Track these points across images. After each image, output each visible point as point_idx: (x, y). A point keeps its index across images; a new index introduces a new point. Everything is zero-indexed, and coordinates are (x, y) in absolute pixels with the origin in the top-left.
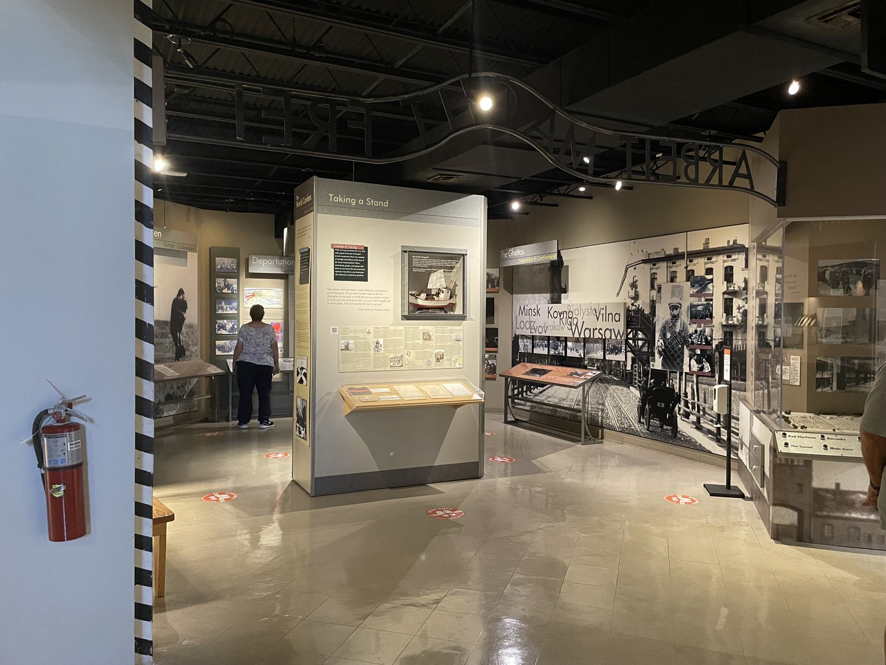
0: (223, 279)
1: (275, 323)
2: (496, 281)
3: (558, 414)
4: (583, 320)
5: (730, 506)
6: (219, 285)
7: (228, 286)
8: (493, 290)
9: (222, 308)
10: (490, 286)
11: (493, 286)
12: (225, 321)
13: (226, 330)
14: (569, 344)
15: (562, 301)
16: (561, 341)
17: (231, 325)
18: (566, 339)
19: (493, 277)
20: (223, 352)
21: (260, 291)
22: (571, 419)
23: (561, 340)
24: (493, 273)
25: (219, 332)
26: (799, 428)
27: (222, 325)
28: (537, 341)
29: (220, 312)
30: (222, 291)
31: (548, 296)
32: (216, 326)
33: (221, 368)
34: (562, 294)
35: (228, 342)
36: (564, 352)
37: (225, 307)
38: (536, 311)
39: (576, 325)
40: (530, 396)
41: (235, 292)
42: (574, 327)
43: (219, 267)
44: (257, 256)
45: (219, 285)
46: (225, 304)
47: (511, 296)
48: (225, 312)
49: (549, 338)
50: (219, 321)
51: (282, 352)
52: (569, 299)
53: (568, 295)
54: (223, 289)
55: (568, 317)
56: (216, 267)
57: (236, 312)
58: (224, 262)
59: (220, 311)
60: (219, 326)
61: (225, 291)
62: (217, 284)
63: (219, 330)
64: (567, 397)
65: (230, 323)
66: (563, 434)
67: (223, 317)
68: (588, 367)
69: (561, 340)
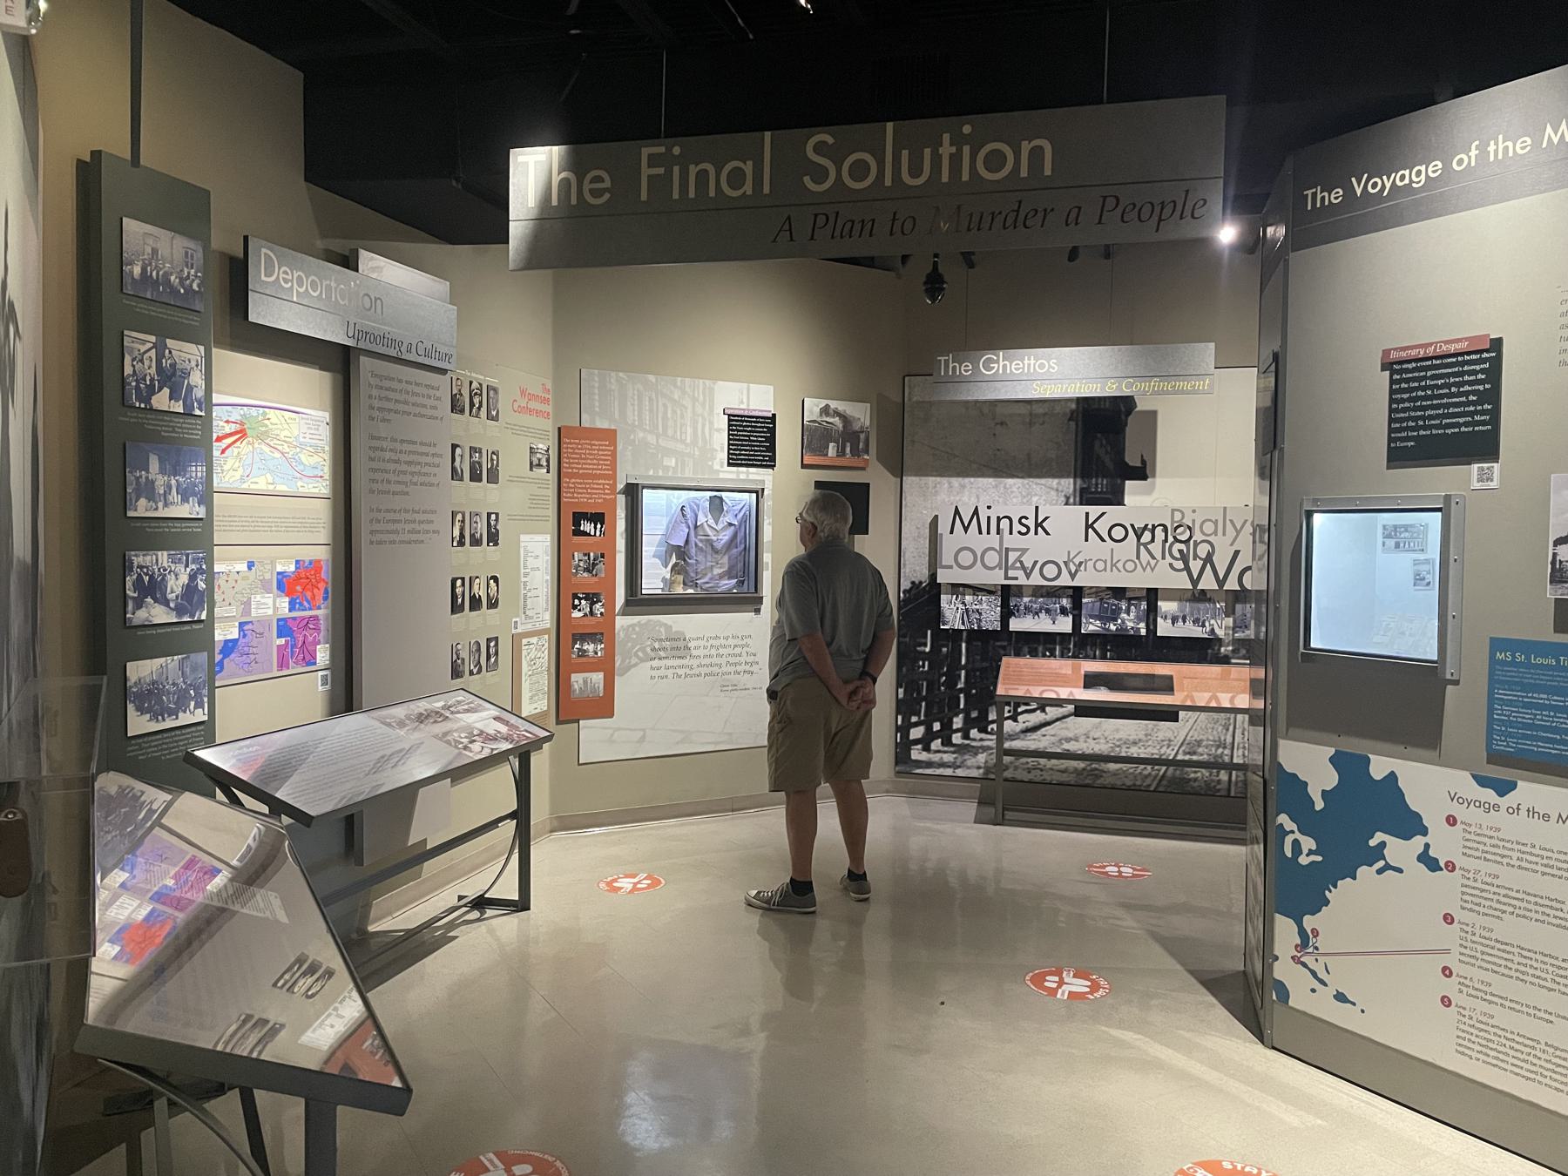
0: (153, 339)
1: (307, 559)
2: (862, 436)
3: (1107, 781)
4: (1235, 547)
5: (199, 936)
6: (138, 366)
7: (171, 378)
8: (856, 462)
9: (148, 490)
10: (848, 450)
11: (856, 452)
12: (163, 557)
13: (166, 603)
14: (1165, 606)
15: (1127, 500)
16: (1130, 599)
17: (184, 579)
18: (1152, 595)
19: (856, 427)
20: (155, 717)
21: (264, 414)
22: (1161, 789)
23: (1128, 595)
24: (857, 416)
25: (141, 616)
26: (259, 757)
27: (152, 577)
28: (1026, 600)
29: (141, 508)
30: (148, 400)
31: (1068, 484)
32: (129, 584)
33: (215, 790)
34: (1127, 482)
35: (172, 662)
36: (1142, 625)
37: (160, 481)
38: (1031, 523)
39: (1209, 559)
40: (981, 740)
41: (197, 412)
42: (1195, 566)
43: (137, 270)
44: (277, 248)
45: (138, 366)
46: (163, 471)
47: (895, 481)
48: (163, 513)
49: (1077, 593)
50: (139, 559)
51: (328, 687)
52: (1155, 495)
53: (1154, 485)
54: (152, 391)
55: (1171, 539)
56: (126, 269)
57: (201, 512)
58: (155, 251)
59: (143, 502)
60: (138, 583)
61: (161, 400)
62: (128, 359)
63: (139, 604)
64: (1146, 735)
65: (180, 568)
66: (1100, 823)
67: (158, 534)
68: (1233, 661)
69: (1128, 595)
